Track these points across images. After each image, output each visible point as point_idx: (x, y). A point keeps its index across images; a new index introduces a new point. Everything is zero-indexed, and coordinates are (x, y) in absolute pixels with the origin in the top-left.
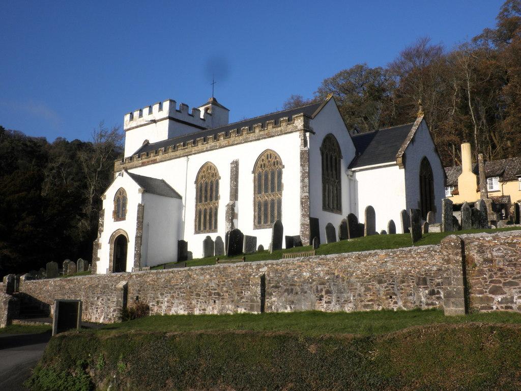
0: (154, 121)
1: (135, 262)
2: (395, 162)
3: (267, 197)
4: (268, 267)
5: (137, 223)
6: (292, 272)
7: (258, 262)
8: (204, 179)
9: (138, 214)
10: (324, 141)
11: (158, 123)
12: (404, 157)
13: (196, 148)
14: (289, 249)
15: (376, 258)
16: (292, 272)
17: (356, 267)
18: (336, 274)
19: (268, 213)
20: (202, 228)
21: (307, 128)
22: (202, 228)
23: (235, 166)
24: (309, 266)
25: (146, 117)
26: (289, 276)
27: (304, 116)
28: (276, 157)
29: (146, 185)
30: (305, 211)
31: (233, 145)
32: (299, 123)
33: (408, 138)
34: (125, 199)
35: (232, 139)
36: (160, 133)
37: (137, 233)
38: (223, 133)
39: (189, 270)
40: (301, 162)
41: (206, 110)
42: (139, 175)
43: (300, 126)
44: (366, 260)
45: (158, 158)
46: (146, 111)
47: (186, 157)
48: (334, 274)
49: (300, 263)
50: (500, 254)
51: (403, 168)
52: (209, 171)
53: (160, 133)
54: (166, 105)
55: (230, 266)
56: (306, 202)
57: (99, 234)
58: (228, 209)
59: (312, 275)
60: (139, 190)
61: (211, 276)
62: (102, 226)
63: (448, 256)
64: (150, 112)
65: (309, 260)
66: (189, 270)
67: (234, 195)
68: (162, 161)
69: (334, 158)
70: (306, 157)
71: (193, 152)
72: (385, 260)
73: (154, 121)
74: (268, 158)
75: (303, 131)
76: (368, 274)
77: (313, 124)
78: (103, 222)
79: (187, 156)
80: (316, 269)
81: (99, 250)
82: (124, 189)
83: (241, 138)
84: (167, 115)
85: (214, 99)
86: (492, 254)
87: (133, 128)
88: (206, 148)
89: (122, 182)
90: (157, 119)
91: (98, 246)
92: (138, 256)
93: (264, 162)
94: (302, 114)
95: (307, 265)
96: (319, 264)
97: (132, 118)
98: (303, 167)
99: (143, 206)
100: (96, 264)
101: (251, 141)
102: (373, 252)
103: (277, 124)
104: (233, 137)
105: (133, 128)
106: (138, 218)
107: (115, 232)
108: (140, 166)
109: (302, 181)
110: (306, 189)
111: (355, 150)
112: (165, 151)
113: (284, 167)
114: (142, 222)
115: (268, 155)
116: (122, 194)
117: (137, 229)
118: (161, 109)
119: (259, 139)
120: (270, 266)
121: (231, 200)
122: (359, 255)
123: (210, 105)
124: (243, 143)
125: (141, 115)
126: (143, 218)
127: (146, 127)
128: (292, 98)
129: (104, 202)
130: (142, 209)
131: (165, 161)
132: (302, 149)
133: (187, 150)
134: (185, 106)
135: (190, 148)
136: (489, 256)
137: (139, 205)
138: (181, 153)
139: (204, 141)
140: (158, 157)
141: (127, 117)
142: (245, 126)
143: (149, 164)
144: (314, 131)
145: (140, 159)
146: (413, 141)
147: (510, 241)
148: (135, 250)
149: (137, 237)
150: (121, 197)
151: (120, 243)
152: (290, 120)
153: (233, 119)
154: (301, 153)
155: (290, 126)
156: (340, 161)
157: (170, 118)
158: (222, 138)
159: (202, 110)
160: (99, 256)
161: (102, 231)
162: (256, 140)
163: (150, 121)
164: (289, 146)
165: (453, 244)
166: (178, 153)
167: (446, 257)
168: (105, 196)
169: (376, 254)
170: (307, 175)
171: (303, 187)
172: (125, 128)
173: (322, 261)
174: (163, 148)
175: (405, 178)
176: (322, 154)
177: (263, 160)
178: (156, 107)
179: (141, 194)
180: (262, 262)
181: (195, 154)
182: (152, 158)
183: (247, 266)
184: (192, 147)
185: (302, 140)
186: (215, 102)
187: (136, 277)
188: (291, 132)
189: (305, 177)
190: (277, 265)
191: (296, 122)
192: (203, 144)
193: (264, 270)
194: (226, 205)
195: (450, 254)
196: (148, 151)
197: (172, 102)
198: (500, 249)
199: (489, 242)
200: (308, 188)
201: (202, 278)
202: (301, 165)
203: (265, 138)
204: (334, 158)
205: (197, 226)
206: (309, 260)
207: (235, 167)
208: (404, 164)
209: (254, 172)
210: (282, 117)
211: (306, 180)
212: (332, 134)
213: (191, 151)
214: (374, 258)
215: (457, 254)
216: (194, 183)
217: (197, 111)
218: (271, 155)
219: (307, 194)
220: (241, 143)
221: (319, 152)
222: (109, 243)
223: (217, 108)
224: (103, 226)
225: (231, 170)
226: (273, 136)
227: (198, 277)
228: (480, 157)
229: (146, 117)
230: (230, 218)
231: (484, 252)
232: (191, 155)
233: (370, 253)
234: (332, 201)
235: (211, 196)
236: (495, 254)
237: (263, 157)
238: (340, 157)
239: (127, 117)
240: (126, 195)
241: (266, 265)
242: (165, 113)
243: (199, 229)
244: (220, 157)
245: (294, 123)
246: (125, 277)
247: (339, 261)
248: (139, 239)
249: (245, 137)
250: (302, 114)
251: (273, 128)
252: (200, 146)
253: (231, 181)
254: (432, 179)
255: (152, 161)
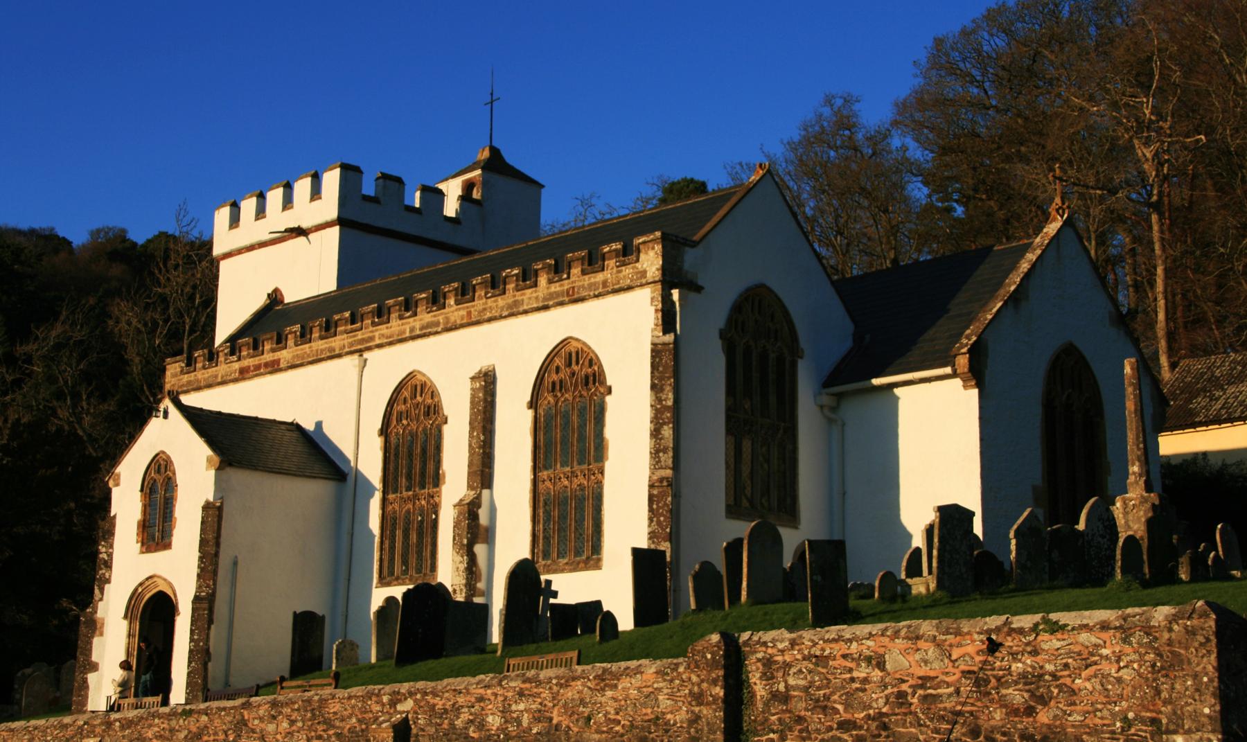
0: (299, 232)
1: (189, 674)
2: (948, 370)
3: (565, 479)
4: (415, 701)
5: (201, 559)
6: (465, 715)
7: (396, 687)
8: (405, 422)
9: (203, 531)
10: (737, 308)
11: (311, 236)
12: (977, 353)
13: (383, 329)
14: (382, 663)
15: (637, 681)
16: (465, 715)
17: (595, 704)
18: (555, 722)
19: (568, 522)
20: (398, 568)
21: (671, 277)
22: (398, 568)
23: (487, 383)
24: (500, 699)
25: (251, 229)
26: (458, 723)
27: (664, 239)
28: (591, 361)
29: (230, 438)
30: (659, 523)
31: (478, 323)
32: (651, 261)
33: (1002, 292)
34: (170, 484)
35: (479, 304)
36: (312, 270)
37: (199, 588)
38: (456, 285)
39: (244, 706)
40: (652, 377)
41: (468, 187)
42: (220, 413)
43: (654, 269)
44: (616, 686)
45: (285, 355)
46: (275, 197)
47: (356, 356)
48: (551, 719)
49: (482, 691)
50: (802, 683)
51: (972, 387)
52: (419, 398)
53: (312, 270)
54: (331, 180)
55: (333, 697)
56: (662, 496)
57: (97, 591)
58: (460, 513)
59: (506, 722)
60: (209, 460)
61: (292, 722)
62: (108, 565)
63: (699, 685)
64: (288, 202)
65: (500, 684)
66: (244, 706)
67: (483, 470)
68: (293, 367)
69: (772, 356)
70: (669, 365)
71: (378, 342)
72: (656, 686)
73: (299, 232)
74: (570, 365)
75: (659, 286)
76: (619, 722)
77: (690, 258)
78: (110, 555)
79: (360, 352)
80: (514, 707)
81: (96, 641)
82: (169, 457)
83: (501, 302)
84: (333, 214)
85: (495, 152)
86: (786, 682)
87: (240, 251)
88: (412, 330)
89: (167, 434)
90: (305, 225)
91: (94, 627)
92: (200, 655)
93: (561, 375)
94: (658, 234)
95: (496, 695)
96: (521, 694)
97: (235, 221)
98: (656, 393)
99: (220, 509)
100: (85, 681)
101: (526, 312)
102: (633, 664)
103: (594, 262)
104: (480, 298)
105: (240, 251)
106: (203, 543)
107: (141, 584)
108: (235, 380)
109: (656, 433)
110: (667, 459)
111: (850, 327)
112: (303, 335)
113: (609, 391)
114: (217, 554)
115: (570, 354)
116: (163, 470)
117: (199, 576)
118: (316, 193)
119: (546, 308)
120: (419, 696)
121: (470, 487)
122: (605, 670)
123: (479, 172)
124: (505, 317)
125: (261, 212)
126: (218, 545)
127: (275, 251)
128: (829, 101)
129: (116, 493)
130: (213, 516)
131: (302, 365)
132: (657, 341)
133: (360, 335)
134: (392, 182)
135: (368, 330)
136: (782, 687)
137: (207, 507)
138: (346, 342)
139: (407, 310)
140: (284, 352)
141: (222, 216)
142: (512, 267)
143: (257, 375)
144: (700, 283)
145: (235, 358)
146: (1015, 299)
147: (818, 653)
148: (192, 640)
149: (197, 599)
150: (160, 479)
151: (154, 612)
152: (628, 253)
153: (557, 212)
154: (652, 351)
155: (627, 271)
156: (794, 365)
157: (341, 221)
158: (452, 302)
159: (452, 190)
160: (94, 658)
161: (108, 581)
162: (538, 309)
163: (286, 231)
164: (620, 326)
165: (709, 656)
166: (337, 342)
167: (696, 689)
168: (119, 475)
169: (638, 671)
170: (671, 417)
171: (656, 453)
172: (217, 251)
173: (528, 685)
174: (297, 328)
175: (981, 418)
176: (730, 350)
177: (558, 369)
178: (303, 187)
179: (213, 472)
180: (405, 687)
181: (380, 346)
182: (268, 357)
183: (369, 695)
184: (374, 324)
185: (656, 311)
186: (496, 164)
187: (123, 728)
188: (629, 288)
189: (664, 423)
190: (435, 694)
191: (642, 256)
192: (401, 318)
193: (407, 706)
194: (457, 500)
195: (702, 681)
196: (276, 323)
197: (350, 173)
198: (800, 671)
199: (782, 651)
200: (671, 454)
201: (271, 728)
202: (653, 387)
203: (562, 304)
204: (772, 356)
205: (386, 564)
206: (500, 684)
207: (487, 383)
208: (977, 375)
209: (533, 404)
210: (608, 242)
211: (667, 432)
212: (762, 286)
213: (372, 339)
214: (633, 681)
215: (714, 682)
216: (525, 405)
217: (434, 196)
218: (577, 353)
219: (669, 473)
220: (502, 317)
221: (718, 344)
222: (126, 617)
223: (499, 180)
224: (110, 567)
225: (473, 397)
226: (582, 300)
227: (263, 725)
228: (747, 445)
229: (277, 219)
230: (465, 541)
231: (773, 677)
232: (369, 349)
233: (628, 668)
234: (763, 485)
235: (423, 474)
236: (791, 681)
237: (557, 361)
238: (796, 352)
239: (222, 216)
240: (174, 474)
241: (411, 694)
242: (329, 207)
243: (391, 573)
244: (508, 345)
245: (638, 261)
246: (94, 726)
247: (561, 686)
248: (204, 604)
249: (510, 301)
250: (658, 234)
251: (584, 273)
252: (395, 325)
253: (472, 428)
254: (1100, 414)
255: (266, 365)
